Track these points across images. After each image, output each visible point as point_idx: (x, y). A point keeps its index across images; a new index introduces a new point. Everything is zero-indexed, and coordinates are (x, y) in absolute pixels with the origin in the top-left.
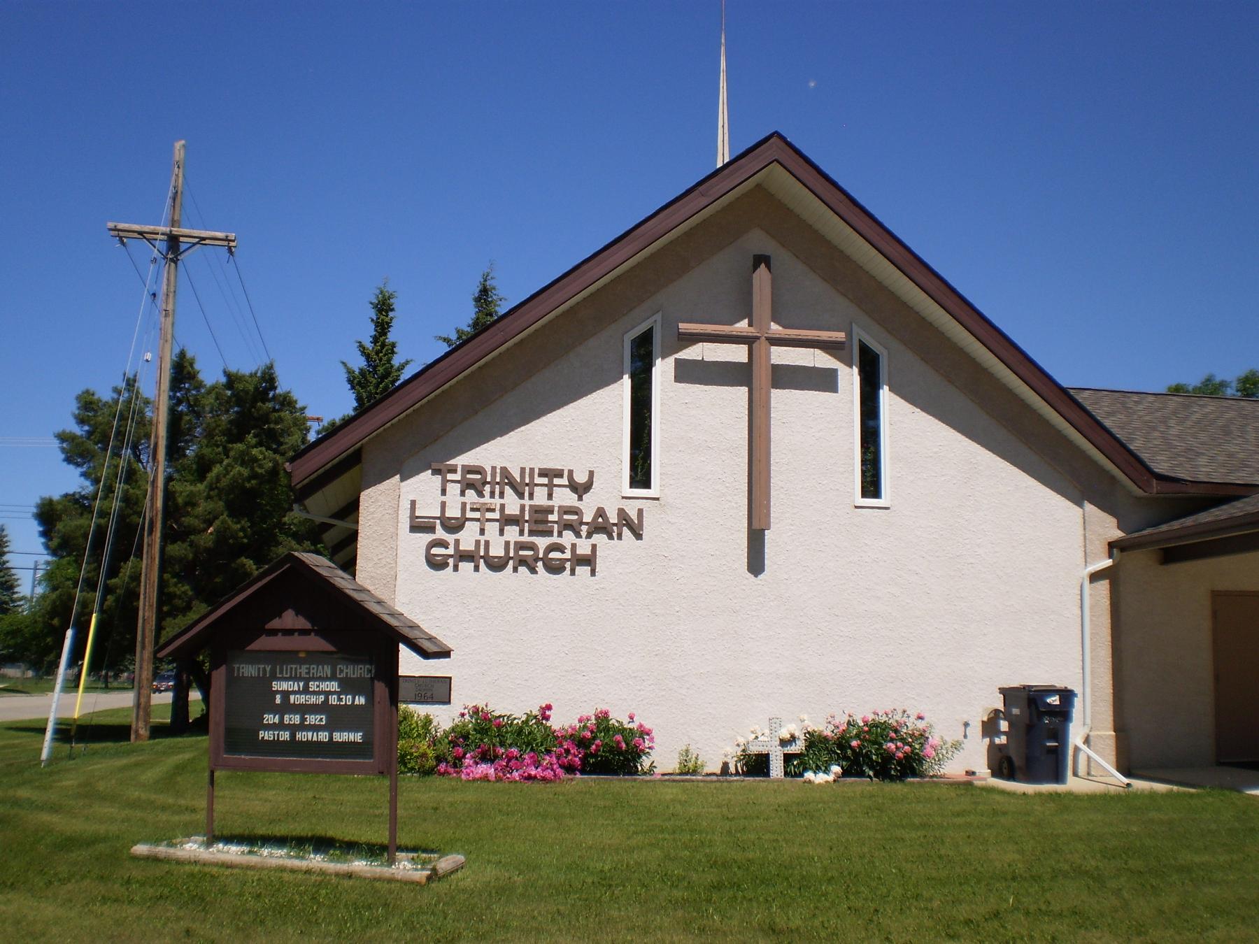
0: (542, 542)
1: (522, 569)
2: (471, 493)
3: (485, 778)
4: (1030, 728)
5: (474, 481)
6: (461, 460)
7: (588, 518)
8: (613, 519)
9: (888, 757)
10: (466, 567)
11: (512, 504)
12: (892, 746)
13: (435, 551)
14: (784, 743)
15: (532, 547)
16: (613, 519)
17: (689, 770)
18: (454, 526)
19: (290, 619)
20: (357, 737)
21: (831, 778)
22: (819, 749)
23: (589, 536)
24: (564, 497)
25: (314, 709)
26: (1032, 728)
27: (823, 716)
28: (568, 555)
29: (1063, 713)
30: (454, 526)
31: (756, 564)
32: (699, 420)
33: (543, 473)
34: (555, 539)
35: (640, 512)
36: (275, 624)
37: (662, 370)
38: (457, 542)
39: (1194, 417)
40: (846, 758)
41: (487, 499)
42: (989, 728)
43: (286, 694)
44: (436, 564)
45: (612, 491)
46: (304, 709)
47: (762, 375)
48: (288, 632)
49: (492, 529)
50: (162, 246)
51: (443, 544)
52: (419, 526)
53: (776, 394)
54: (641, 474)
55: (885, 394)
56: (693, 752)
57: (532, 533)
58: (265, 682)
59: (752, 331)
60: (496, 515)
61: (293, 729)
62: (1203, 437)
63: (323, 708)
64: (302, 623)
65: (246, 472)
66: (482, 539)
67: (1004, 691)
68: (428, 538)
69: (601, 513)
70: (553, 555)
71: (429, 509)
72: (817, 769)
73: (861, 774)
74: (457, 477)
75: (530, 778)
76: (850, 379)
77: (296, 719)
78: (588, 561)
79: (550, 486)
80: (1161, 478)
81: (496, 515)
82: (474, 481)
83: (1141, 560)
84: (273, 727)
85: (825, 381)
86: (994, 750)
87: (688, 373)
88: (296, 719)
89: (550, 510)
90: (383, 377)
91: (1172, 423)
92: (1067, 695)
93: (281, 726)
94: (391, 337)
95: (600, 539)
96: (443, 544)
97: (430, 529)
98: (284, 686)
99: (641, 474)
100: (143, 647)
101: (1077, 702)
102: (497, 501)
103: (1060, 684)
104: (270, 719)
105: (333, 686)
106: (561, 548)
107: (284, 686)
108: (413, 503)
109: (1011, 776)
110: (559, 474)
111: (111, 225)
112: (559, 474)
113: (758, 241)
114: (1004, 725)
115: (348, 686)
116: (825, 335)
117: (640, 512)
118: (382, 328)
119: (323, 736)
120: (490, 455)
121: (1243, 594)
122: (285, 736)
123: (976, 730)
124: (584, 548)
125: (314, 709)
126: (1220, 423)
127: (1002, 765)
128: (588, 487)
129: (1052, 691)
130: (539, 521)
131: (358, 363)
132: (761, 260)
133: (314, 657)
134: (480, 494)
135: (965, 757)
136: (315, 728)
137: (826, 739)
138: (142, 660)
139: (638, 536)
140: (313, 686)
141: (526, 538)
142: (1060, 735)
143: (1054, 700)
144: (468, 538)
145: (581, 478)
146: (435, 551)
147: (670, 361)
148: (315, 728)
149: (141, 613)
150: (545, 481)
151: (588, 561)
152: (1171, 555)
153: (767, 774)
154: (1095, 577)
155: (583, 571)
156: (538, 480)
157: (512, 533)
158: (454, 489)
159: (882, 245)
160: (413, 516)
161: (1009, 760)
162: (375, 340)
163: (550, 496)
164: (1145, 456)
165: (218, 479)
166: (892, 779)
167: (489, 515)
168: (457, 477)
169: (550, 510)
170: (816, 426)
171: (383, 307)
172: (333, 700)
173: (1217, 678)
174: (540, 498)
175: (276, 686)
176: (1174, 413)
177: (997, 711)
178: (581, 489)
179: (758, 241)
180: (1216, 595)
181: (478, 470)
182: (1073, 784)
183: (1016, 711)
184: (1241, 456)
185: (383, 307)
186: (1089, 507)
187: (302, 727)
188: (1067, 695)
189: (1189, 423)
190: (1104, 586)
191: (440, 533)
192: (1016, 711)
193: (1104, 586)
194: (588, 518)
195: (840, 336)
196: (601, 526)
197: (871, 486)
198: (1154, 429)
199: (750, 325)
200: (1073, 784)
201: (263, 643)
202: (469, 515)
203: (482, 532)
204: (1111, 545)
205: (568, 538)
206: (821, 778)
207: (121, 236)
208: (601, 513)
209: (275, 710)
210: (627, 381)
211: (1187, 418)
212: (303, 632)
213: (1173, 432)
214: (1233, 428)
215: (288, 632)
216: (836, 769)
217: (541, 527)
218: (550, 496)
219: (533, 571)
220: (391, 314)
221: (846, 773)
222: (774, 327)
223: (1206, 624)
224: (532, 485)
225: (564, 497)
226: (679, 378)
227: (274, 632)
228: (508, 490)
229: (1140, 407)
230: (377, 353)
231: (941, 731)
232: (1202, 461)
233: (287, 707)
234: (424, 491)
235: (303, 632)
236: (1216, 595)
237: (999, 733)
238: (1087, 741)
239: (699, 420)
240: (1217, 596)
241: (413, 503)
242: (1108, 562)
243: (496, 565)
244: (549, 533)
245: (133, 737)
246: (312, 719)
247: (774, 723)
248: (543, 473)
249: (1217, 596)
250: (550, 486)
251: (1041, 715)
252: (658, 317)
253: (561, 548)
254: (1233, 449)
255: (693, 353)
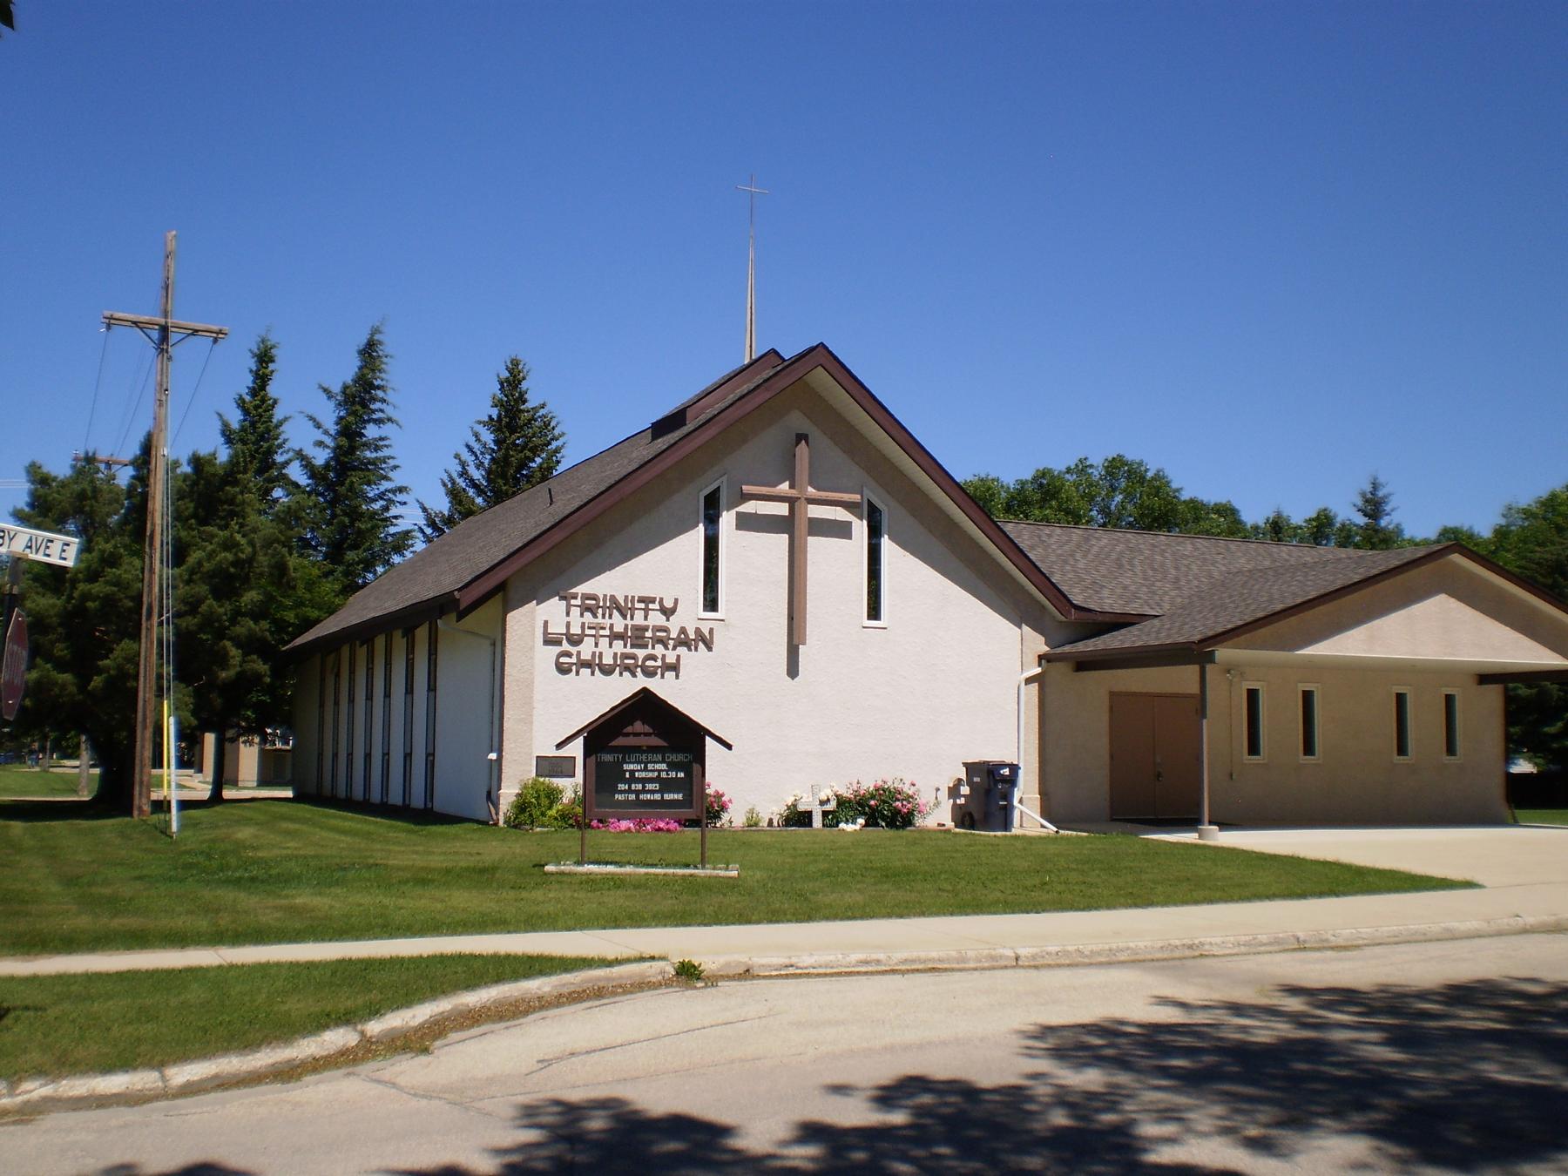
0: (641, 653)
1: (626, 674)
2: (588, 615)
3: (629, 830)
4: (988, 792)
5: (590, 606)
6: (581, 589)
7: (674, 635)
8: (692, 636)
9: (897, 812)
10: (585, 672)
11: (619, 624)
12: (898, 804)
13: (562, 660)
14: (822, 803)
15: (634, 657)
16: (692, 636)
17: (752, 824)
18: (575, 641)
19: (638, 726)
20: (680, 796)
21: (857, 827)
22: (848, 807)
23: (674, 648)
24: (656, 619)
25: (651, 780)
26: (987, 791)
27: (842, 784)
28: (659, 663)
29: (1012, 781)
30: (575, 641)
31: (793, 671)
32: (752, 558)
33: (641, 600)
34: (649, 651)
35: (711, 631)
36: (629, 729)
37: (727, 520)
38: (579, 653)
39: (1095, 549)
40: (864, 814)
41: (600, 620)
42: (954, 792)
43: (632, 772)
44: (563, 670)
45: (691, 615)
46: (644, 781)
47: (801, 526)
48: (636, 735)
49: (604, 642)
50: (155, 335)
51: (569, 655)
52: (550, 641)
53: (813, 541)
54: (711, 603)
55: (885, 542)
56: (757, 809)
57: (633, 646)
58: (619, 764)
59: (793, 493)
60: (607, 632)
61: (637, 793)
62: (1103, 570)
63: (658, 779)
64: (647, 729)
65: (230, 556)
66: (597, 651)
67: (965, 764)
68: (557, 649)
69: (683, 631)
70: (649, 663)
71: (557, 628)
72: (847, 822)
73: (877, 825)
74: (578, 602)
75: (660, 829)
76: (860, 528)
77: (640, 787)
78: (675, 668)
79: (646, 610)
80: (1077, 608)
81: (607, 632)
82: (590, 606)
83: (1062, 670)
84: (621, 792)
85: (843, 530)
86: (955, 807)
87: (747, 523)
88: (640, 787)
89: (646, 629)
90: (262, 438)
91: (1078, 556)
92: (1014, 768)
93: (630, 791)
94: (273, 390)
95: (682, 650)
96: (569, 655)
97: (558, 643)
98: (631, 767)
99: (711, 603)
100: (145, 727)
101: (1021, 772)
102: (607, 622)
103: (1008, 761)
104: (622, 787)
105: (664, 766)
106: (654, 658)
107: (631, 767)
108: (546, 623)
109: (972, 827)
110: (653, 600)
111: (107, 313)
112: (653, 600)
113: (804, 425)
114: (965, 790)
115: (673, 766)
116: (846, 497)
117: (711, 631)
118: (261, 380)
119: (657, 797)
120: (602, 585)
121: (1134, 694)
122: (632, 797)
123: (944, 794)
124: (671, 659)
125: (651, 780)
126: (1114, 556)
127: (965, 818)
128: (673, 611)
129: (1004, 765)
130: (637, 637)
131: (235, 418)
132: (801, 437)
133: (653, 749)
134: (595, 616)
135: (938, 815)
136: (652, 792)
137: (850, 801)
138: (143, 739)
139: (710, 649)
140: (650, 766)
141: (629, 650)
142: (1008, 796)
143: (1006, 771)
144: (586, 650)
145: (669, 604)
146: (562, 660)
147: (733, 512)
148: (652, 792)
149: (141, 694)
150: (642, 606)
151: (675, 668)
152: (1083, 664)
153: (810, 825)
154: (1028, 681)
155: (670, 675)
156: (638, 605)
157: (618, 646)
158: (575, 612)
159: (894, 433)
160: (545, 633)
161: (971, 815)
162: (254, 392)
163: (646, 618)
164: (1064, 589)
165: (200, 563)
166: (898, 828)
167: (602, 632)
168: (578, 602)
169: (646, 629)
170: (837, 563)
171: (264, 358)
172: (664, 775)
173: (1112, 757)
174: (639, 619)
175: (625, 767)
176: (1078, 546)
177: (960, 780)
178: (668, 612)
179: (797, 421)
180: (1112, 694)
181: (594, 597)
182: (1016, 831)
183: (977, 779)
184: (1133, 588)
185: (264, 358)
186: (1025, 628)
187: (644, 791)
188: (1014, 768)
189: (1091, 557)
190: (1035, 686)
191: (566, 646)
192: (977, 779)
193: (1035, 686)
194: (674, 635)
195: (856, 498)
196: (683, 641)
197: (874, 611)
198: (1066, 562)
199: (792, 486)
200: (1016, 831)
201: (620, 741)
202: (588, 632)
203: (596, 645)
204: (1040, 657)
205: (659, 650)
206: (850, 827)
207: (110, 322)
208: (683, 631)
209: (625, 781)
210: (701, 527)
211: (1089, 551)
212: (646, 734)
213: (1081, 565)
214: (1124, 561)
215: (636, 735)
216: (861, 821)
217: (640, 642)
218: (646, 618)
219: (634, 675)
220: (271, 366)
221: (867, 825)
222: (810, 489)
223: (1105, 717)
224: (633, 609)
225: (656, 619)
226: (739, 527)
227: (628, 735)
228: (615, 613)
229: (1052, 540)
230: (257, 407)
231: (925, 797)
232: (1106, 593)
233: (633, 779)
234: (551, 613)
235: (646, 734)
236: (1112, 694)
237: (960, 796)
238: (1021, 801)
239: (752, 558)
240: (1114, 695)
241: (546, 623)
242: (1039, 670)
243: (607, 671)
244: (646, 646)
245: (136, 813)
246: (649, 786)
247: (814, 789)
248: (641, 600)
249: (1114, 695)
250: (646, 610)
251: (996, 782)
252: (724, 478)
253: (654, 658)
254: (1127, 582)
255: (750, 507)
